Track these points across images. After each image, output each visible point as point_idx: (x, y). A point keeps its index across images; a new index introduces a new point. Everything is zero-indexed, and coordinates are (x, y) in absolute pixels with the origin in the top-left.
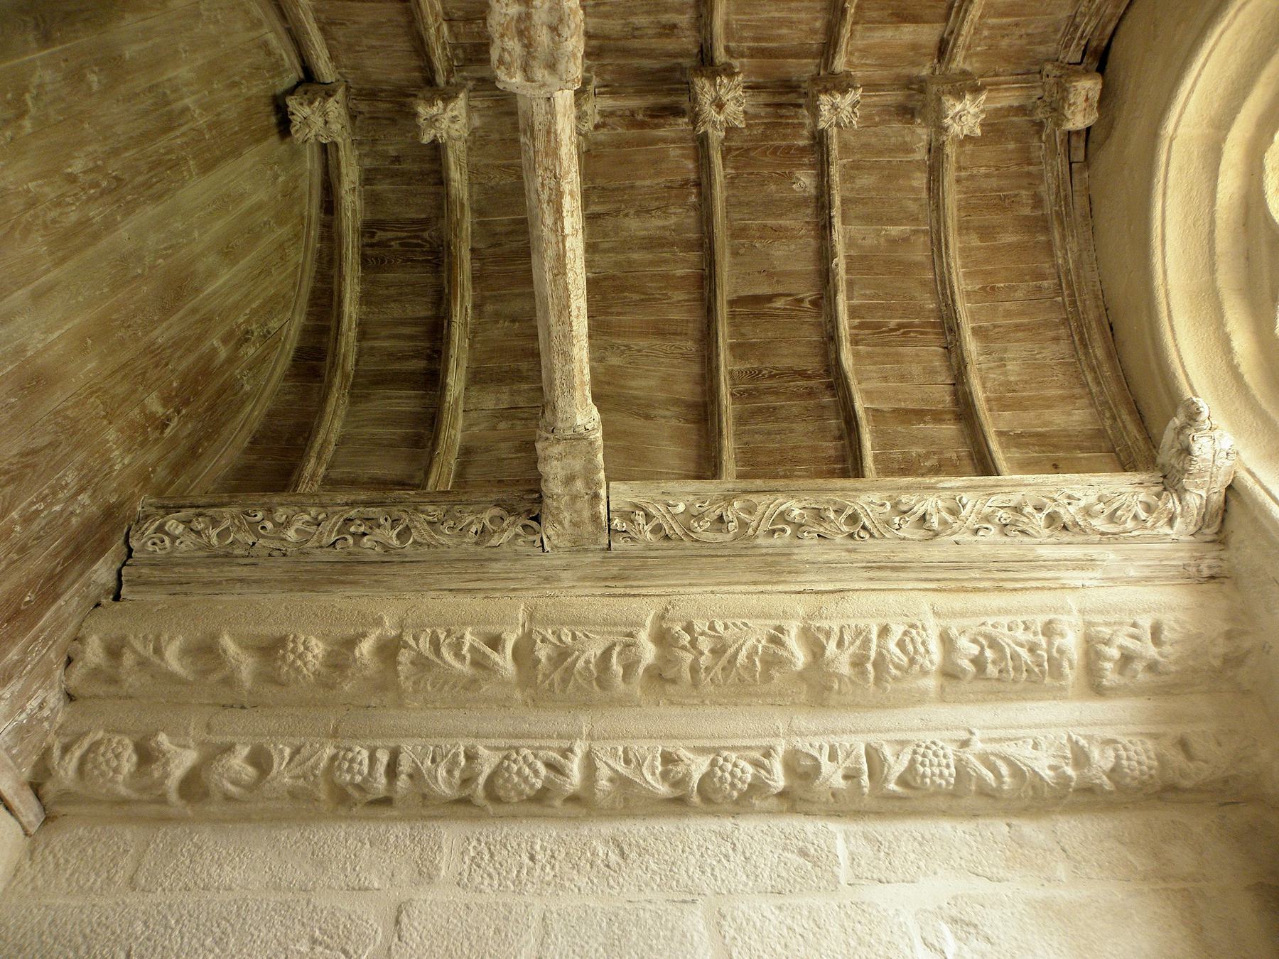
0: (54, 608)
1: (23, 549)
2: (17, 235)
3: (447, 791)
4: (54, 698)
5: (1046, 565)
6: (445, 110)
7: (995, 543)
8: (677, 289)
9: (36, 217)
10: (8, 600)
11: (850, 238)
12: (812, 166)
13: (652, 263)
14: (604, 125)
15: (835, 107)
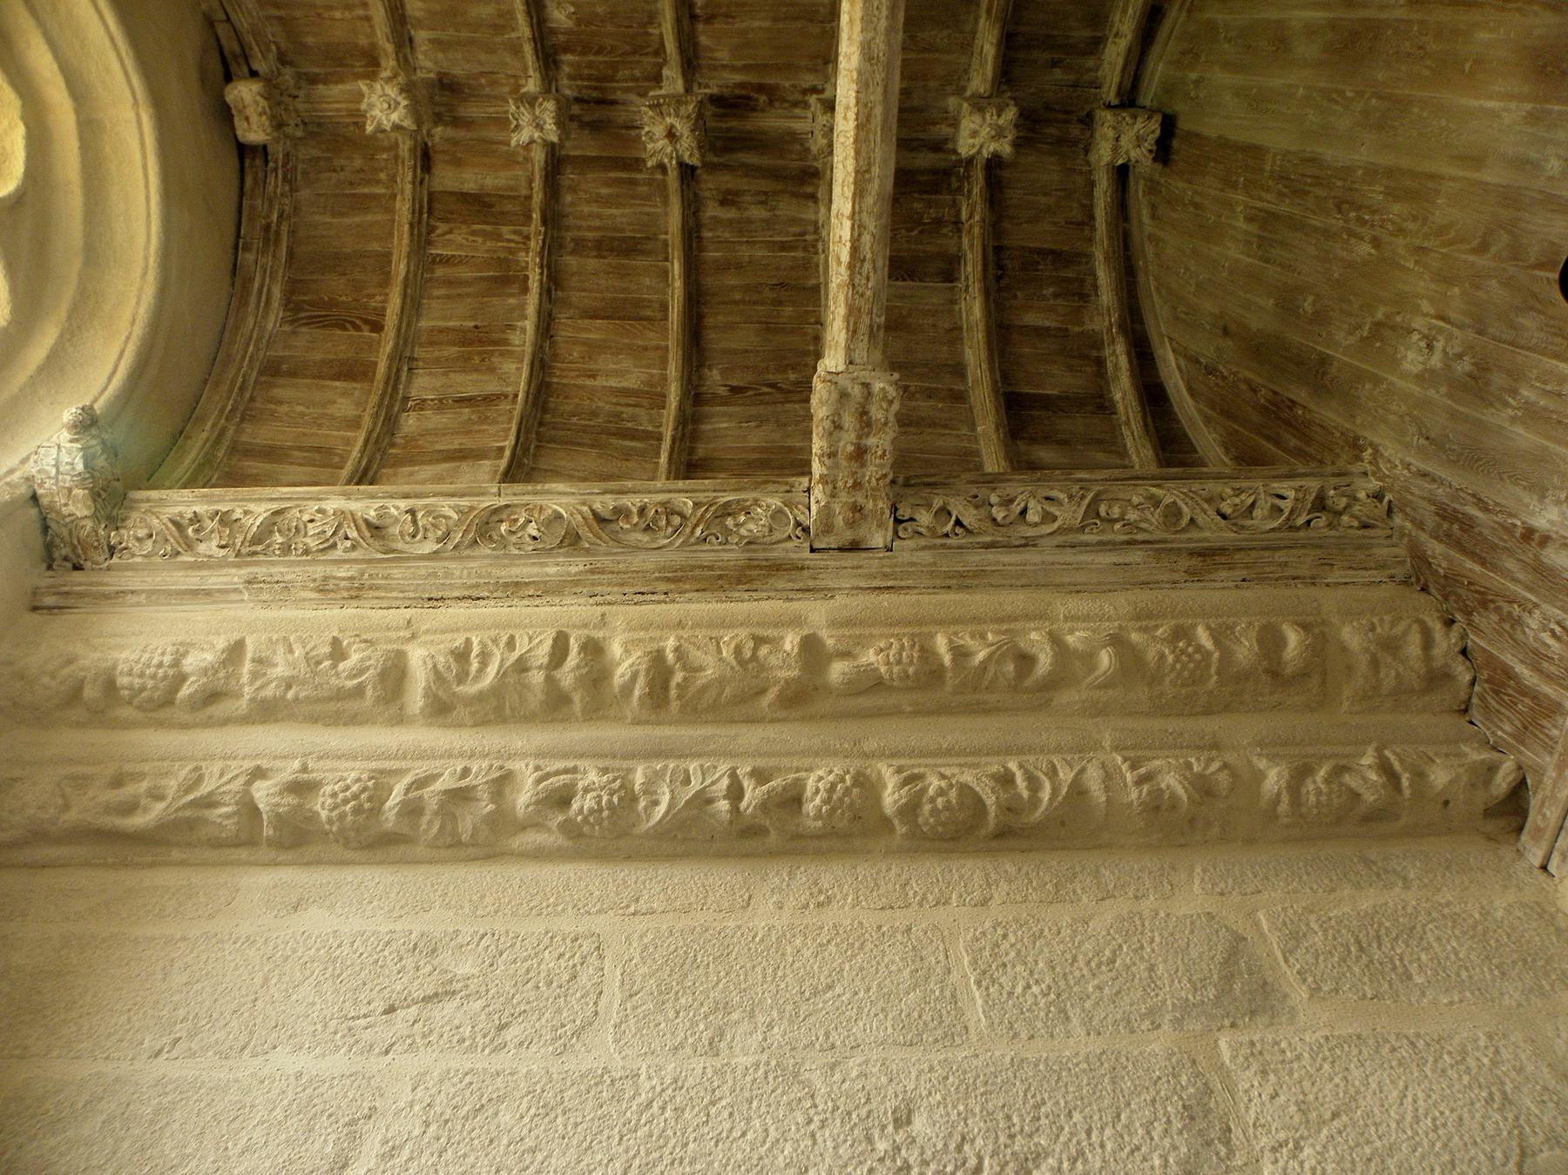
2: (1452, 234)
6: (981, 147)
12: (553, 31)
14: (805, 92)
15: (540, 127)
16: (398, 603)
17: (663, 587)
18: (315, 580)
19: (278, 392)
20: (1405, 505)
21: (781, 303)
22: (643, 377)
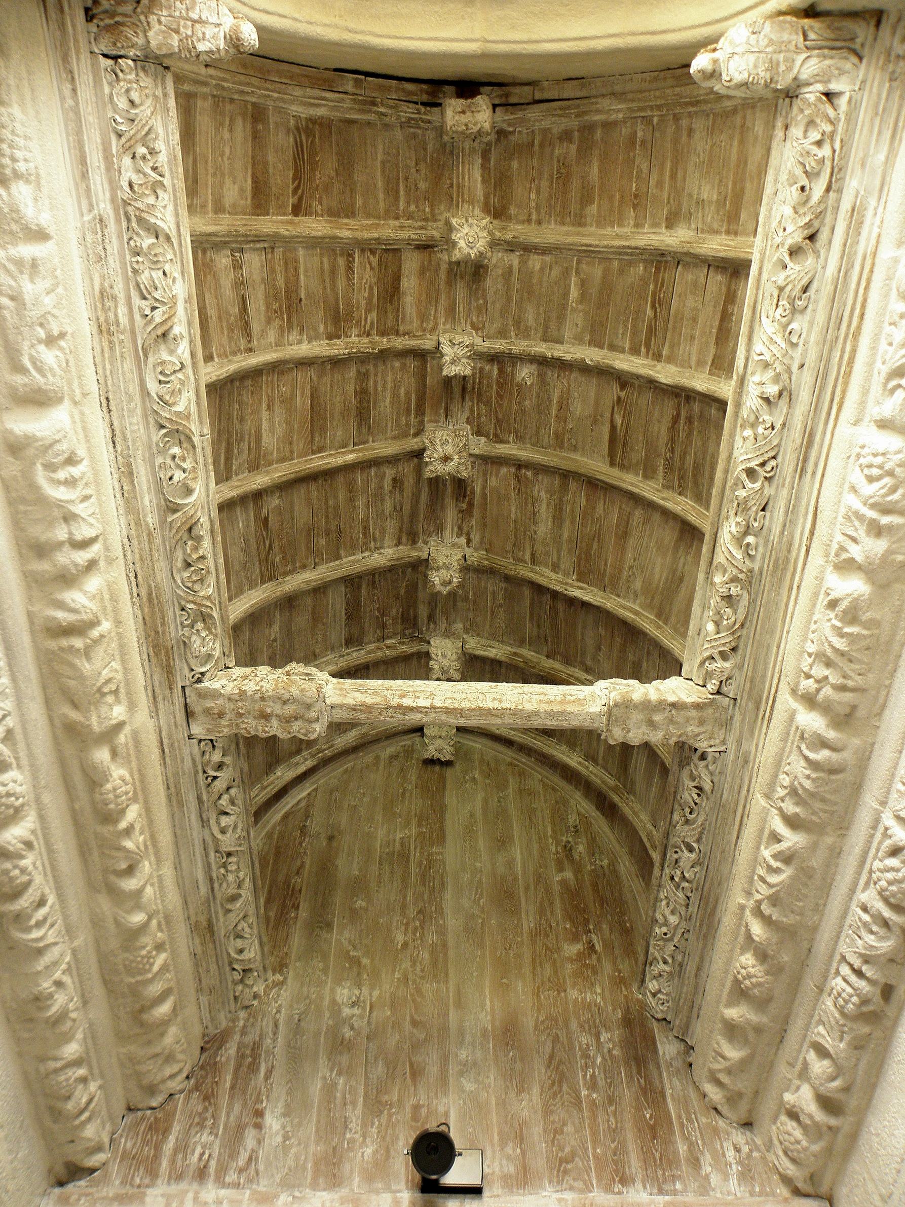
0: (669, 1100)
1: (611, 1100)
2: (419, 1000)
3: (889, 943)
4: (739, 1137)
5: (844, 272)
7: (811, 323)
8: (595, 508)
9: (414, 982)
10: (639, 1130)
11: (575, 339)
12: (514, 365)
13: (573, 521)
15: (453, 362)
16: (100, 371)
17: (144, 593)
18: (112, 287)
19: (239, 122)
20: (254, 1017)
21: (328, 534)
22: (271, 447)
